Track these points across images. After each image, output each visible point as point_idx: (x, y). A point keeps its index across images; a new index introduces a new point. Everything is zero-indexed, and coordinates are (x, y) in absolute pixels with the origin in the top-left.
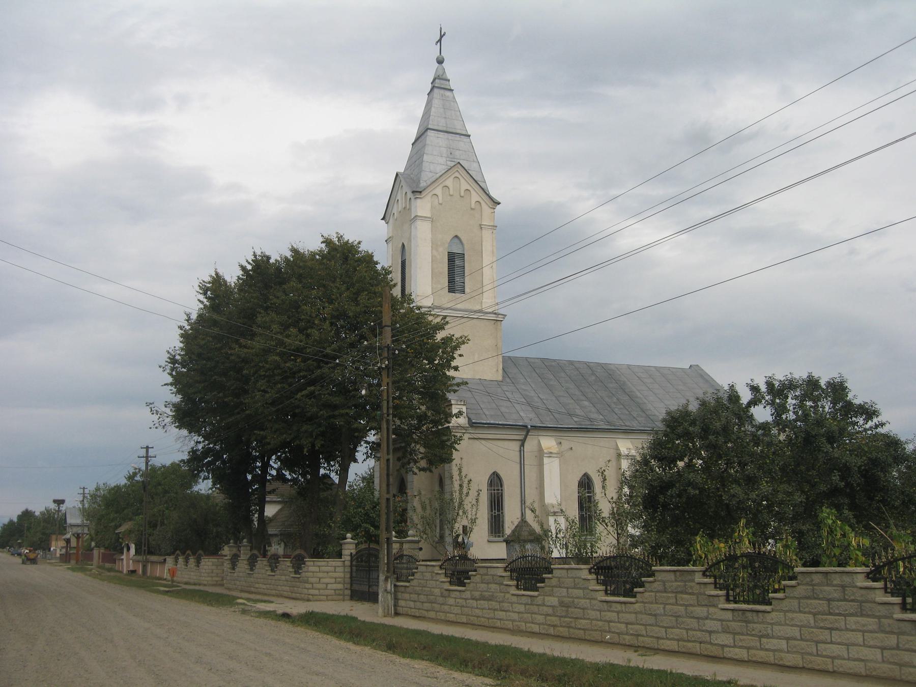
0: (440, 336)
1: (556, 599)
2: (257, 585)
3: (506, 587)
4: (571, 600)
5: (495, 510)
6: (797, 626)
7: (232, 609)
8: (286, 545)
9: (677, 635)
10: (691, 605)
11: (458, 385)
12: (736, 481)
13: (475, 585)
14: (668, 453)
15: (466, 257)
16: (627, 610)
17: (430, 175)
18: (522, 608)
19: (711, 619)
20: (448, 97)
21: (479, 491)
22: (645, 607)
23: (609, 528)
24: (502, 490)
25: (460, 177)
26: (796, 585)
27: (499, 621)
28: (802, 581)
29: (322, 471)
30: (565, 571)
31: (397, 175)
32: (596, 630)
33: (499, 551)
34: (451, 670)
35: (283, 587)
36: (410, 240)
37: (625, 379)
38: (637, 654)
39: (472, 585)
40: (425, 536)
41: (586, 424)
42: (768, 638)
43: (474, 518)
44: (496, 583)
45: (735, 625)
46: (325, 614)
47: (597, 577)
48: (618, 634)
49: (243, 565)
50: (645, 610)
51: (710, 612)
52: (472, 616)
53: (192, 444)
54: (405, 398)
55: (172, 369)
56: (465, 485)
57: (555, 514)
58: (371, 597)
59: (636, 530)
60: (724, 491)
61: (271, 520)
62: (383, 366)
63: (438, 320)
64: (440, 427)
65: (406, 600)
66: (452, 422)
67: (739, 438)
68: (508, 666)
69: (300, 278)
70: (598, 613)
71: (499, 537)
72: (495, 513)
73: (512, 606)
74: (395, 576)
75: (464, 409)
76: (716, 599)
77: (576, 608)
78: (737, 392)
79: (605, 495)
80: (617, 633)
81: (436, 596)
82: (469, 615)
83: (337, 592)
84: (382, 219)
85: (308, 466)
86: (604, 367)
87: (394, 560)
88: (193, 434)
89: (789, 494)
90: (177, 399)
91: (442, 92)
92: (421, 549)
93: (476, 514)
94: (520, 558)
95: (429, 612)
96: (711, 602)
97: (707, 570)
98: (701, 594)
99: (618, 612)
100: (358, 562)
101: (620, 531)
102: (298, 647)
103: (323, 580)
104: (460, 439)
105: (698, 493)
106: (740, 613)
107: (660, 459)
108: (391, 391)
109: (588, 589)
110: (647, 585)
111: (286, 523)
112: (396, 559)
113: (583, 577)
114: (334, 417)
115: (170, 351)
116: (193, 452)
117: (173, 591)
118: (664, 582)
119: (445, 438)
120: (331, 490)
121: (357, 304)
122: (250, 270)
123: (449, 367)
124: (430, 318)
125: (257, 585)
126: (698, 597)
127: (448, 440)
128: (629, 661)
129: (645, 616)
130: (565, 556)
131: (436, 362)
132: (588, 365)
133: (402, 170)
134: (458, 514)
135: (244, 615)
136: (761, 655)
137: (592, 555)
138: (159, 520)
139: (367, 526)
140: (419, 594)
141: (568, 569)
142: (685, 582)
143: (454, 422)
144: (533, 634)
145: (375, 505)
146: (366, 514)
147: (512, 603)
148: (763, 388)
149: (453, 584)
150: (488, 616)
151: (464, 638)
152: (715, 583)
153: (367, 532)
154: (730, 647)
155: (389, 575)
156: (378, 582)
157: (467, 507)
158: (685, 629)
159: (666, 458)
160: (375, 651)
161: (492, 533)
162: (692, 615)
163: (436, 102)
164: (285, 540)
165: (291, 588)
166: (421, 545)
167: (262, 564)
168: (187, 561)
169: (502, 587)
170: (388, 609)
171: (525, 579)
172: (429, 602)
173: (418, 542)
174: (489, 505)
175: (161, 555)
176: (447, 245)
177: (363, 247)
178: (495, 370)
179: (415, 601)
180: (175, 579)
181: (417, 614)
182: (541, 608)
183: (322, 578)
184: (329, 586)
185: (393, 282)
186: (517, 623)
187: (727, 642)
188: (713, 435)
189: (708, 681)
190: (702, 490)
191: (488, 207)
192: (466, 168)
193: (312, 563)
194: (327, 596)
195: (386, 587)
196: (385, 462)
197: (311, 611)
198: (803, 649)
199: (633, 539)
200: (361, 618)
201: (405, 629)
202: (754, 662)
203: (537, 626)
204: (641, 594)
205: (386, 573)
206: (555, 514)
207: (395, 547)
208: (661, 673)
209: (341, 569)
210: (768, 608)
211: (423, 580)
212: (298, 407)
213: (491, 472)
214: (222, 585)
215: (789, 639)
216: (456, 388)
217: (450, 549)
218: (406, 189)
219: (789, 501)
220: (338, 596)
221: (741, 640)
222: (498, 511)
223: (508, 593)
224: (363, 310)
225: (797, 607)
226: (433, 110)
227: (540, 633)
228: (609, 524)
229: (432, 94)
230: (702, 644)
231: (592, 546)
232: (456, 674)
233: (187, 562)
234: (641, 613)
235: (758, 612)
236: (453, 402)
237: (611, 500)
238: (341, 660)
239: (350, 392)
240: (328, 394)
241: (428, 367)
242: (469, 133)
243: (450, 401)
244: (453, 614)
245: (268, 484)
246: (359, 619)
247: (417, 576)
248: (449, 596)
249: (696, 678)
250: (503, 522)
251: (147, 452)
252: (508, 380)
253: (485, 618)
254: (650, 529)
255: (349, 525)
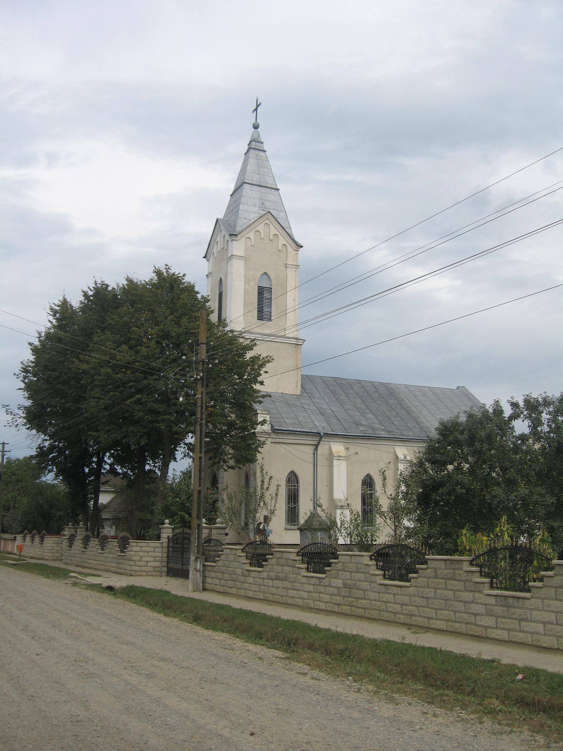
0: (249, 355)
1: (341, 581)
2: (89, 561)
3: (298, 569)
4: (354, 582)
5: (291, 503)
6: (553, 612)
7: (65, 582)
8: (117, 528)
9: (446, 616)
10: (459, 590)
11: (263, 397)
12: (498, 484)
13: (271, 566)
14: (440, 457)
15: (273, 291)
16: (402, 593)
17: (246, 221)
18: (311, 588)
19: (477, 603)
20: (262, 156)
21: (278, 486)
22: (418, 590)
23: (389, 521)
24: (298, 486)
25: (269, 223)
26: (554, 575)
27: (291, 598)
28: (559, 572)
29: (147, 467)
30: (349, 557)
31: (217, 220)
32: (375, 609)
33: (294, 537)
34: (247, 642)
35: (110, 563)
36: (226, 276)
37: (403, 397)
38: (411, 631)
39: (268, 567)
40: (231, 523)
41: (370, 432)
42: (528, 622)
43: (272, 508)
44: (290, 566)
45: (498, 610)
46: (144, 588)
47: (377, 563)
48: (395, 613)
49: (78, 544)
50: (418, 593)
51: (476, 597)
52: (268, 593)
53: (40, 441)
54: (218, 407)
55: (25, 378)
56: (266, 481)
57: (342, 507)
58: (184, 574)
59: (411, 523)
60: (488, 492)
61: (105, 506)
62: (199, 377)
63: (248, 342)
64: (246, 433)
65: (212, 578)
66: (258, 428)
67: (501, 446)
68: (297, 640)
69: (132, 303)
70: (377, 594)
71: (294, 525)
72: (291, 505)
73: (302, 586)
74: (204, 557)
75: (268, 418)
76: (481, 585)
77: (357, 589)
78: (501, 407)
79: (385, 492)
80: (393, 613)
81: (239, 575)
82: (265, 593)
83: (156, 569)
84: (204, 258)
85: (136, 462)
86: (386, 386)
87: (204, 543)
88: (40, 433)
89: (542, 495)
90: (29, 403)
91: (257, 152)
92: (227, 534)
93: (275, 507)
94: (311, 545)
95: (232, 589)
96: (476, 588)
97: (473, 560)
98: (467, 581)
99: (394, 595)
100: (174, 544)
101: (397, 524)
102: (115, 618)
103: (143, 559)
104: (264, 443)
105: (465, 492)
106: (503, 598)
107: (433, 462)
108: (204, 399)
109: (369, 573)
110: (421, 572)
111: (118, 510)
112: (205, 542)
113: (364, 563)
114: (157, 421)
115: (24, 362)
116: (40, 448)
117: (19, 564)
118: (435, 569)
119: (251, 442)
120: (156, 483)
121: (179, 325)
122: (91, 296)
123: (256, 382)
124: (241, 340)
125: (89, 561)
126: (465, 584)
127: (253, 444)
128: (404, 638)
129: (417, 598)
130: (349, 543)
131: (245, 377)
132: (372, 384)
133: (221, 217)
134: (259, 505)
135: (74, 587)
136: (519, 637)
137: (372, 543)
138: (12, 504)
139: (183, 513)
140: (223, 573)
141: (351, 555)
142: (454, 569)
143: (259, 428)
144: (319, 611)
145: (190, 496)
146: (182, 504)
147: (302, 583)
148: (521, 404)
149: (253, 566)
150: (282, 594)
151: (260, 613)
152: (481, 572)
153: (182, 518)
154: (493, 628)
155: (198, 556)
156: (189, 562)
157: (267, 499)
158: (453, 611)
159: (438, 461)
160: (182, 623)
161: (288, 522)
162: (459, 599)
163: (252, 161)
164: (116, 523)
165: (118, 565)
166: (227, 531)
167: (94, 543)
168: (33, 540)
169: (294, 569)
170: (197, 585)
171: (314, 562)
172: (232, 581)
173: (224, 528)
174: (287, 499)
175: (13, 534)
176: (257, 280)
177: (187, 279)
178: (295, 386)
179: (220, 579)
180: (22, 553)
181: (222, 590)
182: (328, 588)
183: (143, 557)
184: (149, 564)
185: (211, 309)
186: (306, 601)
187: (489, 624)
188: (478, 442)
189: (474, 659)
190: (468, 490)
191: (293, 250)
192: (275, 217)
193: (135, 544)
194: (147, 572)
195: (196, 566)
196: (198, 459)
197: (131, 585)
198: (558, 632)
199: (408, 531)
200: (174, 592)
201: (210, 603)
202: (514, 642)
203: (324, 604)
204: (415, 580)
205: (196, 553)
206: (342, 507)
207: (205, 532)
208: (432, 650)
209: (159, 550)
210: (527, 595)
211: (227, 561)
212: (127, 411)
213: (289, 471)
214: (61, 560)
215: (546, 624)
216: (261, 399)
217: (252, 535)
218: (225, 233)
219: (543, 501)
220: (156, 573)
221: (502, 623)
222: (294, 504)
223: (299, 574)
224: (184, 331)
225: (553, 595)
226: (249, 167)
227: (326, 610)
228: (387, 517)
229: (248, 154)
230: (467, 625)
231: (372, 535)
232: (251, 647)
233: (33, 540)
234: (415, 596)
235: (518, 598)
236: (259, 411)
237: (390, 497)
238: (150, 631)
239: (171, 400)
240: (153, 401)
241: (238, 381)
242: (278, 188)
243: (256, 411)
244: (252, 591)
245: (102, 477)
246: (172, 593)
247: (222, 557)
248: (249, 576)
249: (463, 656)
250: (298, 513)
251: (3, 447)
252: (305, 394)
253: (279, 595)
254: (423, 522)
255: (168, 513)
